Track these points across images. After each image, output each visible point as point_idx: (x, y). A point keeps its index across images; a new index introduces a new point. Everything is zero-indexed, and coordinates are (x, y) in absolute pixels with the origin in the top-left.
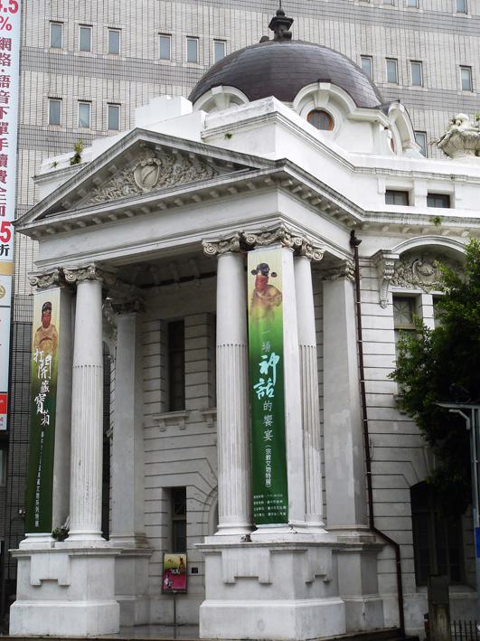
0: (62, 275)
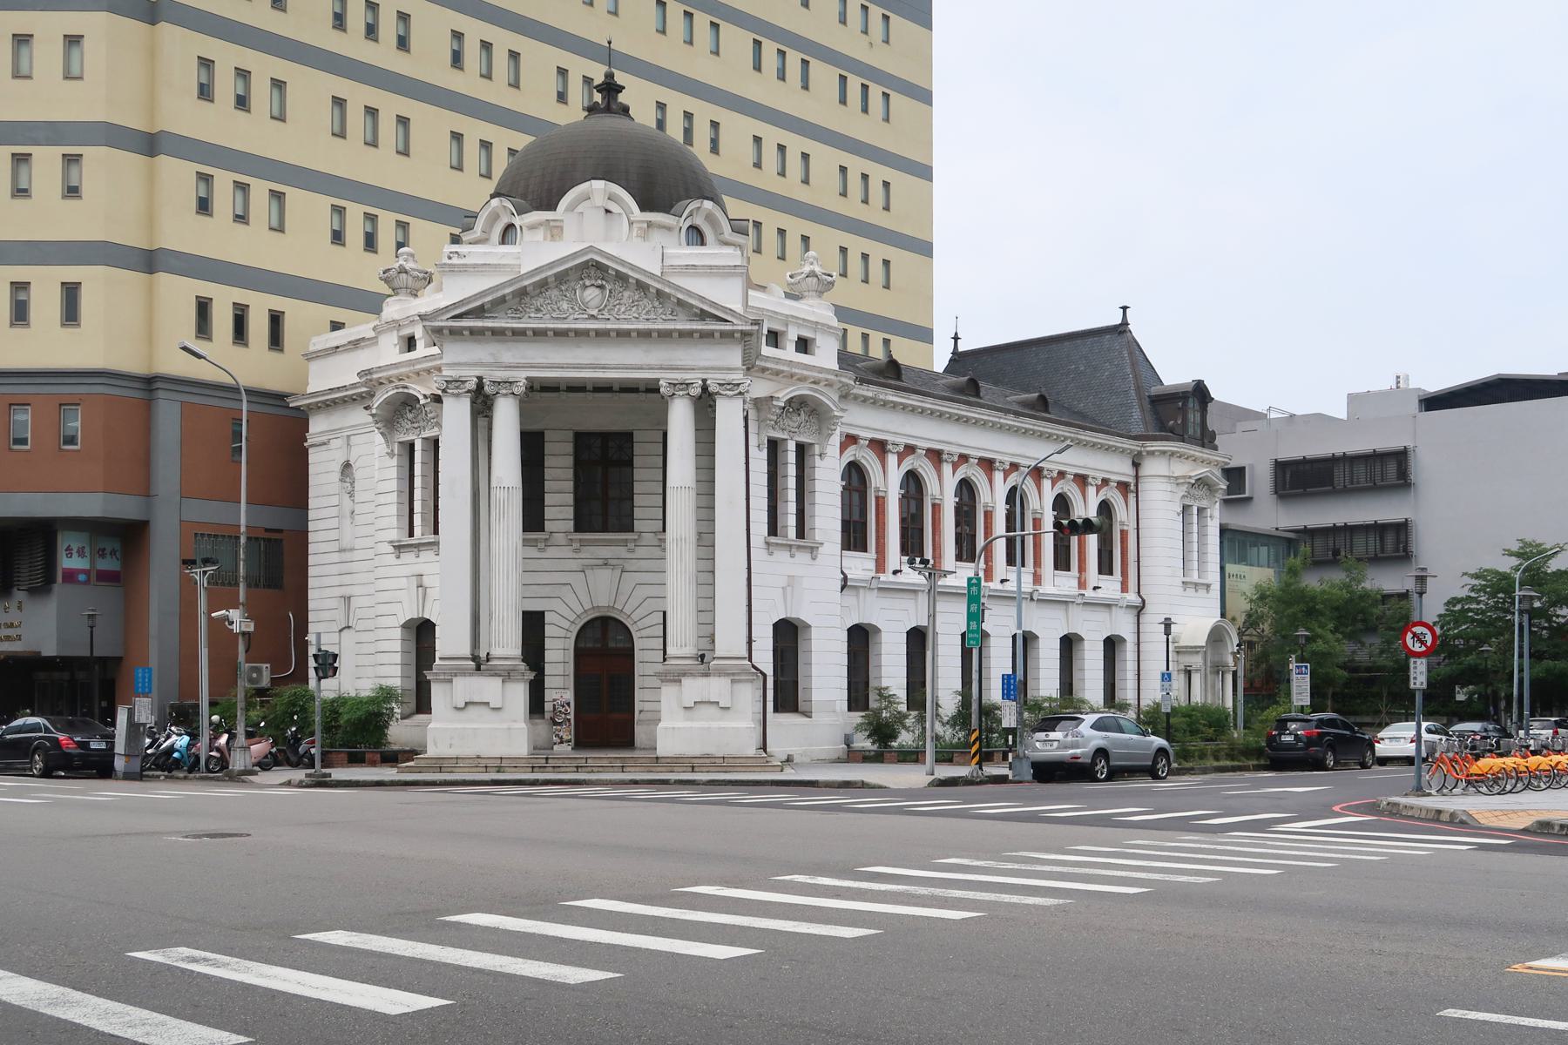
0: (480, 385)
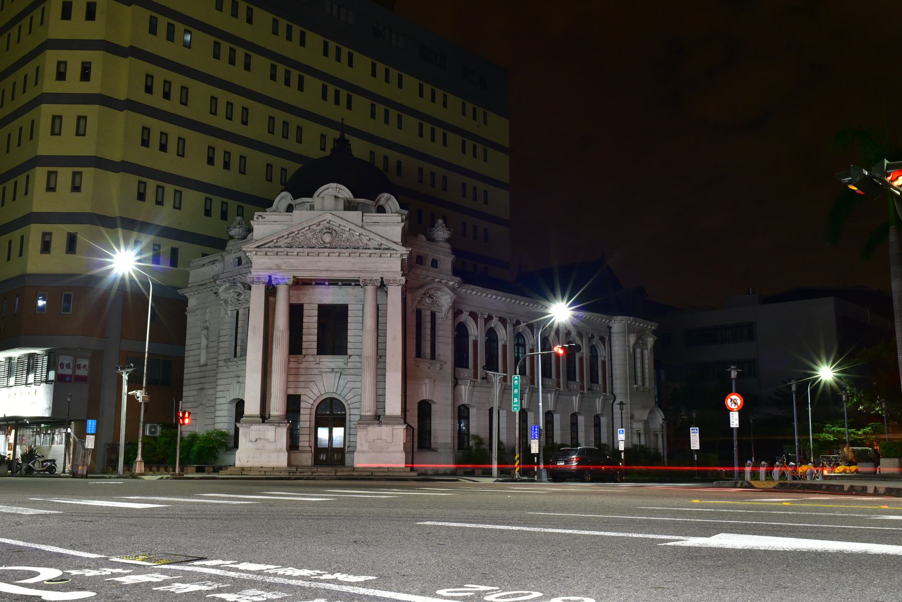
0: (270, 280)
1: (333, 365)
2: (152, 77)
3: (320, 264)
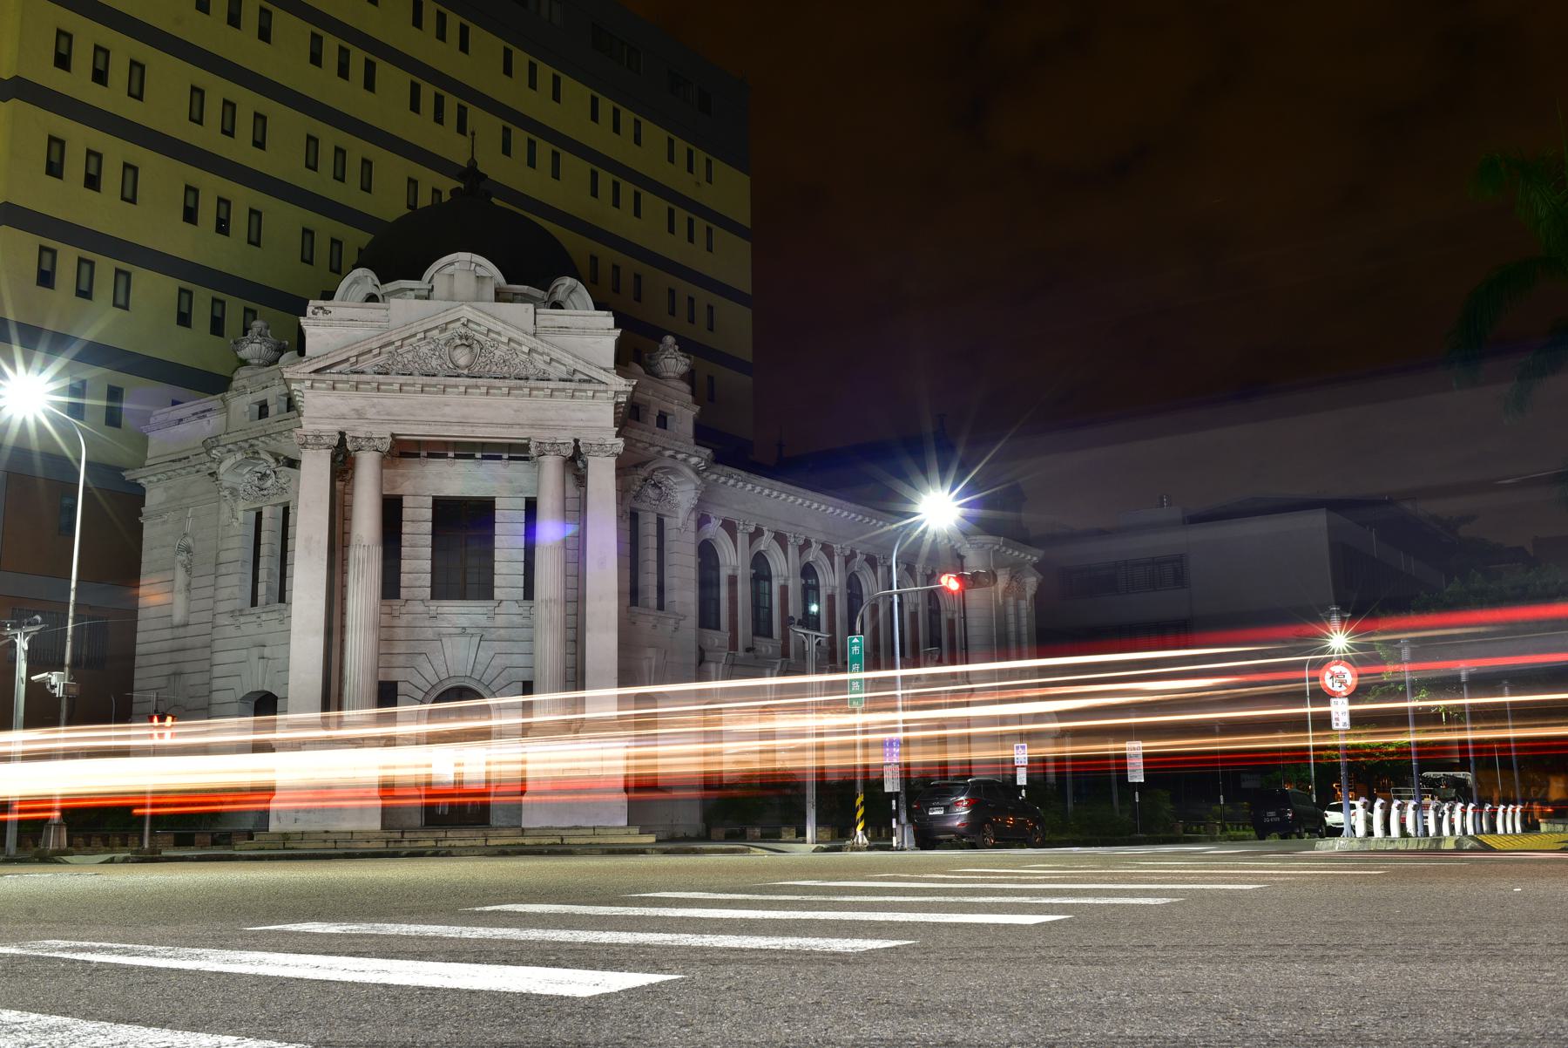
1: (463, 621)
2: (70, 37)
3: (447, 410)
